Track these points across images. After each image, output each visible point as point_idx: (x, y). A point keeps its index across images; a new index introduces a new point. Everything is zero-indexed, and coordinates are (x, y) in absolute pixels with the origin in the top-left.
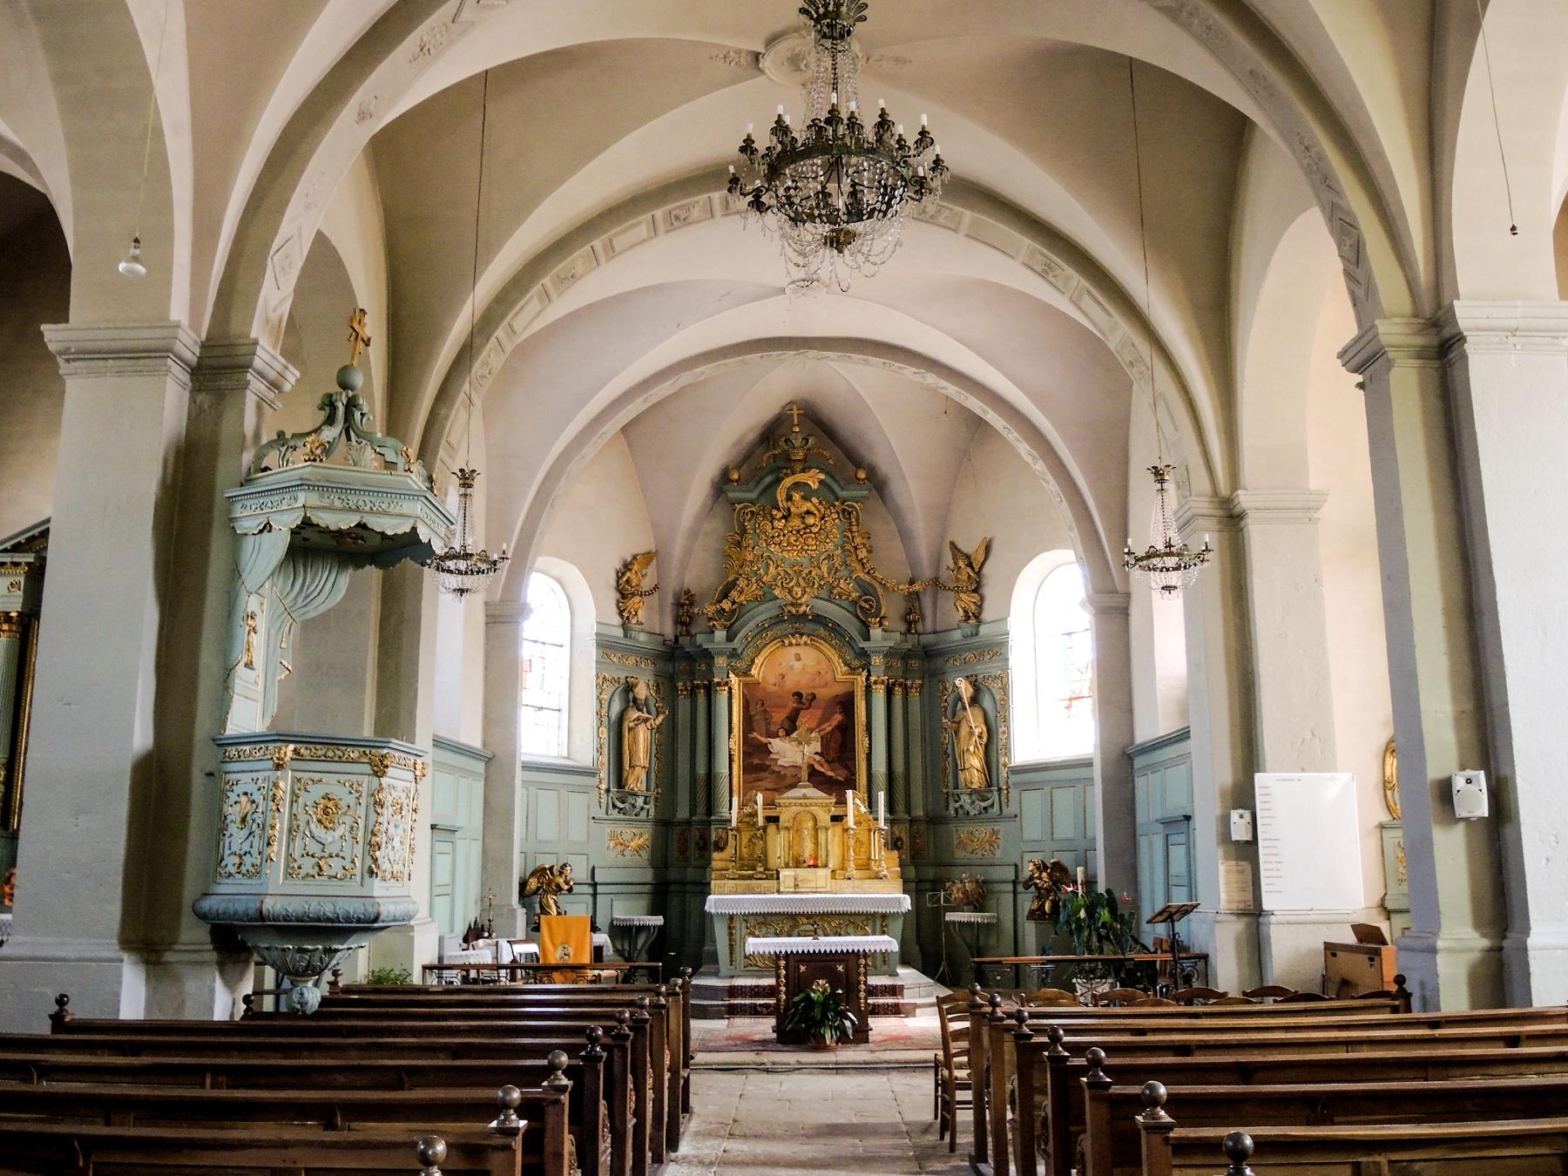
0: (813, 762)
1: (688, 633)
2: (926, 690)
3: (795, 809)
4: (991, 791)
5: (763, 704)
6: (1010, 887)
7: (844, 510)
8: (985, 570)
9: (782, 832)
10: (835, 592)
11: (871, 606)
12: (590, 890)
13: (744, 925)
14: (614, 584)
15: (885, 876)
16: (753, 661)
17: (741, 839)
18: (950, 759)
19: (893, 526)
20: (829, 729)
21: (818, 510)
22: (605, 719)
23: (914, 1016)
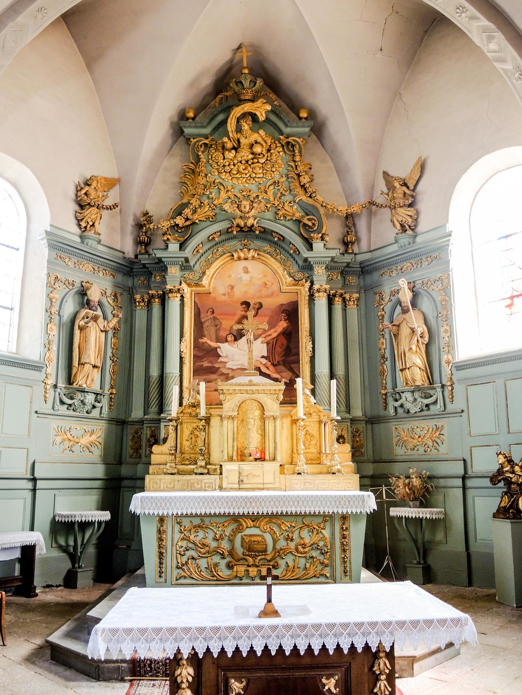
0: (259, 365)
1: (147, 252)
2: (362, 303)
3: (239, 398)
4: (434, 389)
5: (213, 312)
6: (459, 482)
7: (288, 143)
8: (419, 188)
9: (225, 422)
10: (280, 213)
11: (314, 224)
12: (30, 485)
13: (177, 528)
14: (74, 197)
15: (339, 471)
16: (204, 273)
17: (182, 430)
18: (388, 363)
19: (331, 164)
20: (275, 335)
21: (266, 142)
22: (56, 318)
23: (412, 675)
